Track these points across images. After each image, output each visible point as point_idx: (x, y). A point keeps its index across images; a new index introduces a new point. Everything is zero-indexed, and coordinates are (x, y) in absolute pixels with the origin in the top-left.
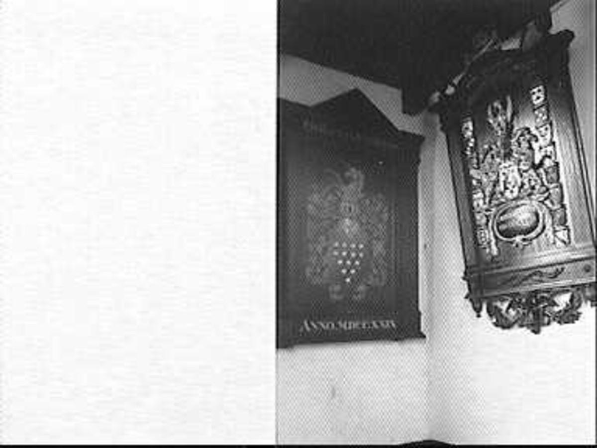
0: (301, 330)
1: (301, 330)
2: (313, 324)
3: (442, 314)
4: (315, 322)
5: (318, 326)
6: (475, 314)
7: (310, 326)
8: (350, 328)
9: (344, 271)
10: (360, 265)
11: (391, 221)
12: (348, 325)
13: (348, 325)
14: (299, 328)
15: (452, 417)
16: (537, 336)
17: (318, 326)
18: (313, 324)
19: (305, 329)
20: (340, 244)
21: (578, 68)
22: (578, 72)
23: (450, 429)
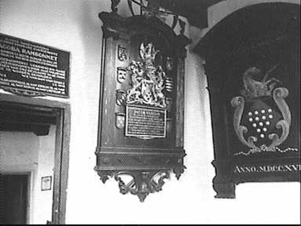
0: (235, 171)
1: (235, 171)
2: (242, 169)
3: (232, 165)
4: (243, 167)
5: (245, 170)
6: (176, 178)
7: (241, 170)
8: (269, 170)
9: (268, 123)
10: (272, 110)
11: (179, 143)
12: (267, 169)
13: (267, 169)
14: (234, 170)
15: (73, 14)
16: (121, 195)
17: (245, 170)
18: (242, 169)
19: (238, 171)
20: (253, 113)
21: (22, 3)
22: (22, 5)
23: (93, 50)
